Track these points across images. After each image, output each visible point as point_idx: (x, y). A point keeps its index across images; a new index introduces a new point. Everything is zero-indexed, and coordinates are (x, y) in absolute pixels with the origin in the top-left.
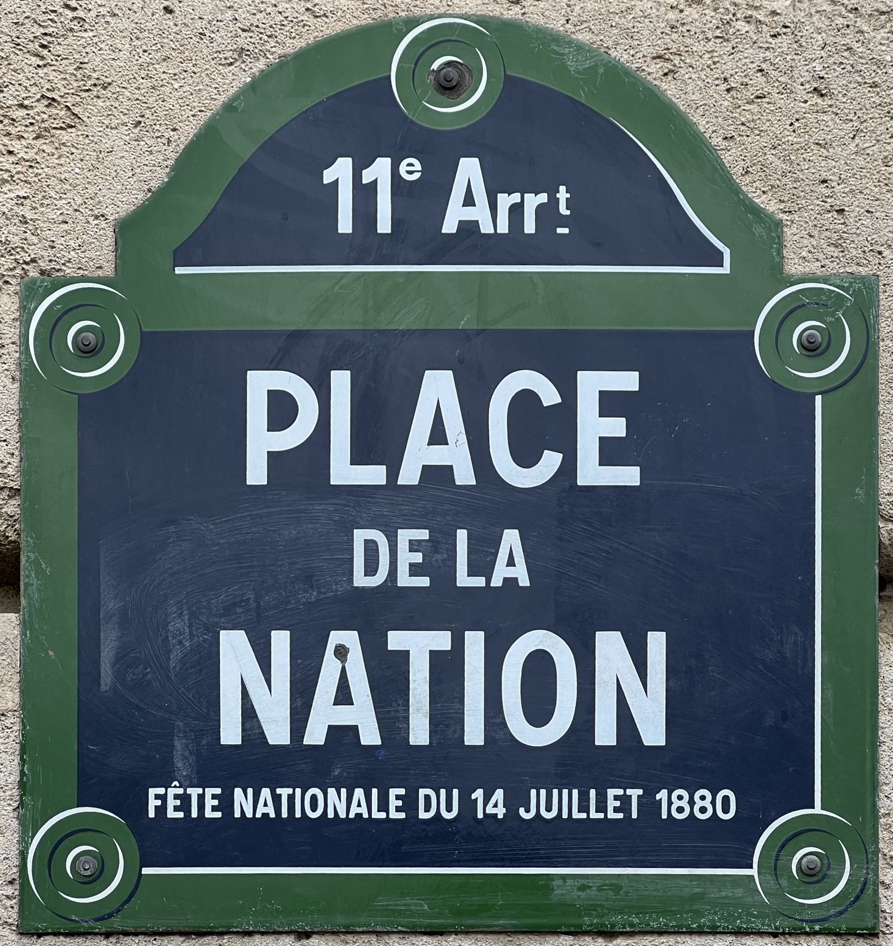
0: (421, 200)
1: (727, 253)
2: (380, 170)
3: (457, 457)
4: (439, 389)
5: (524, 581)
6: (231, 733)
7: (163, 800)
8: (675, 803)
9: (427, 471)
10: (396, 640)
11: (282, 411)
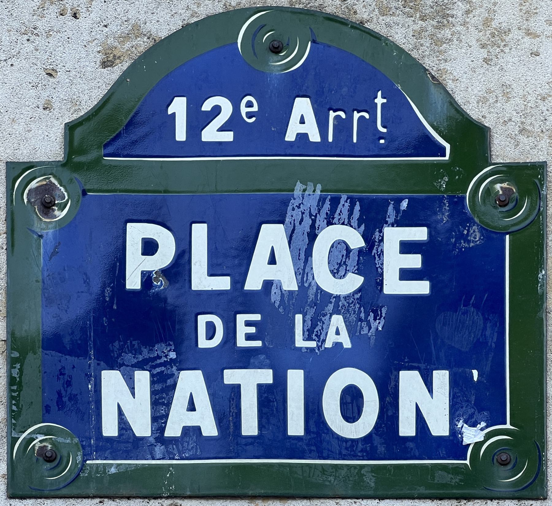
1: (448, 146)
4: (272, 236)
5: (347, 344)
6: (110, 428)
9: (186, 430)
10: (231, 376)
11: (150, 247)
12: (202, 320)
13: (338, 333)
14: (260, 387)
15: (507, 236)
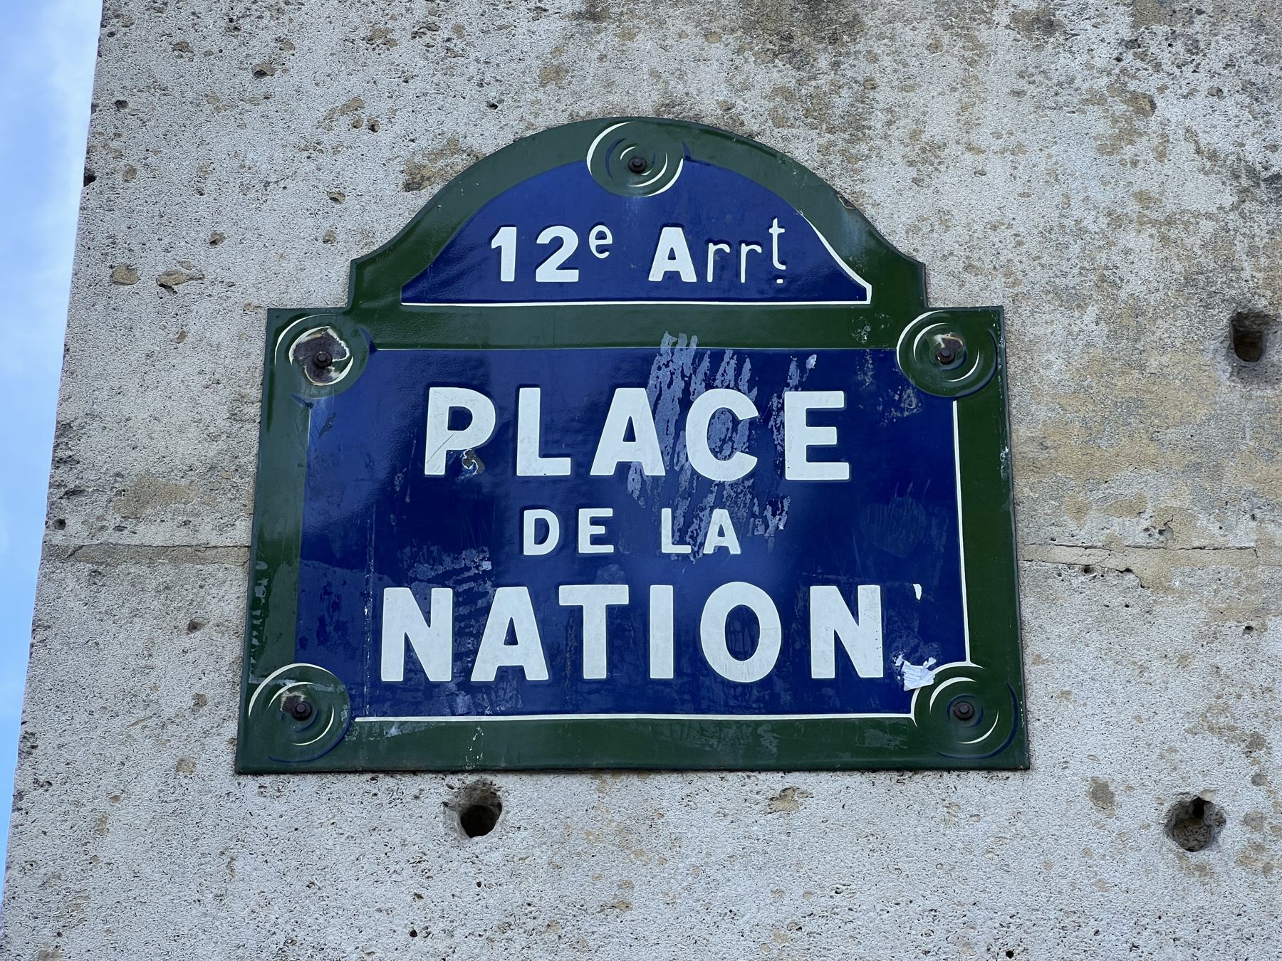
0: (625, 268)
4: (630, 404)
5: (735, 549)
10: (569, 595)
14: (610, 609)
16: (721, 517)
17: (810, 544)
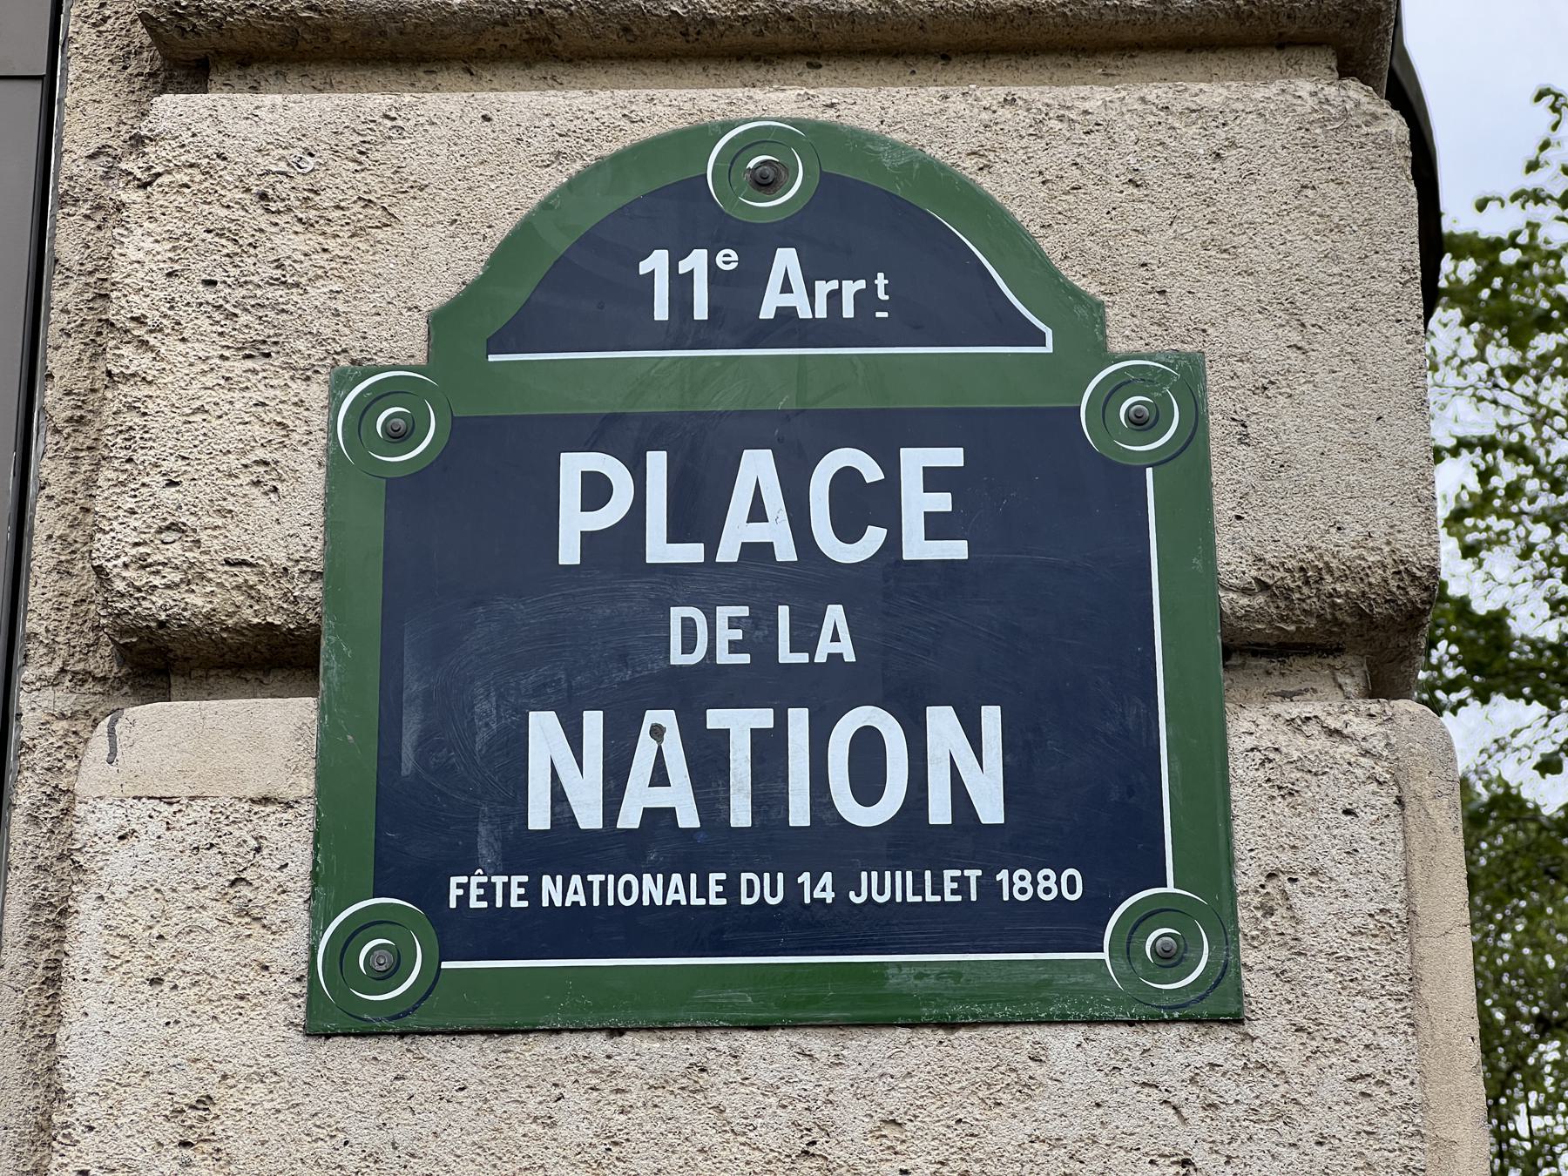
2: (696, 261)
3: (778, 534)
4: (758, 468)
5: (850, 657)
6: (539, 817)
7: (466, 889)
8: (1017, 884)
11: (596, 491)
12: (677, 614)
13: (835, 638)
14: (755, 733)
15: (1149, 471)
16: (835, 614)
17: (917, 643)
